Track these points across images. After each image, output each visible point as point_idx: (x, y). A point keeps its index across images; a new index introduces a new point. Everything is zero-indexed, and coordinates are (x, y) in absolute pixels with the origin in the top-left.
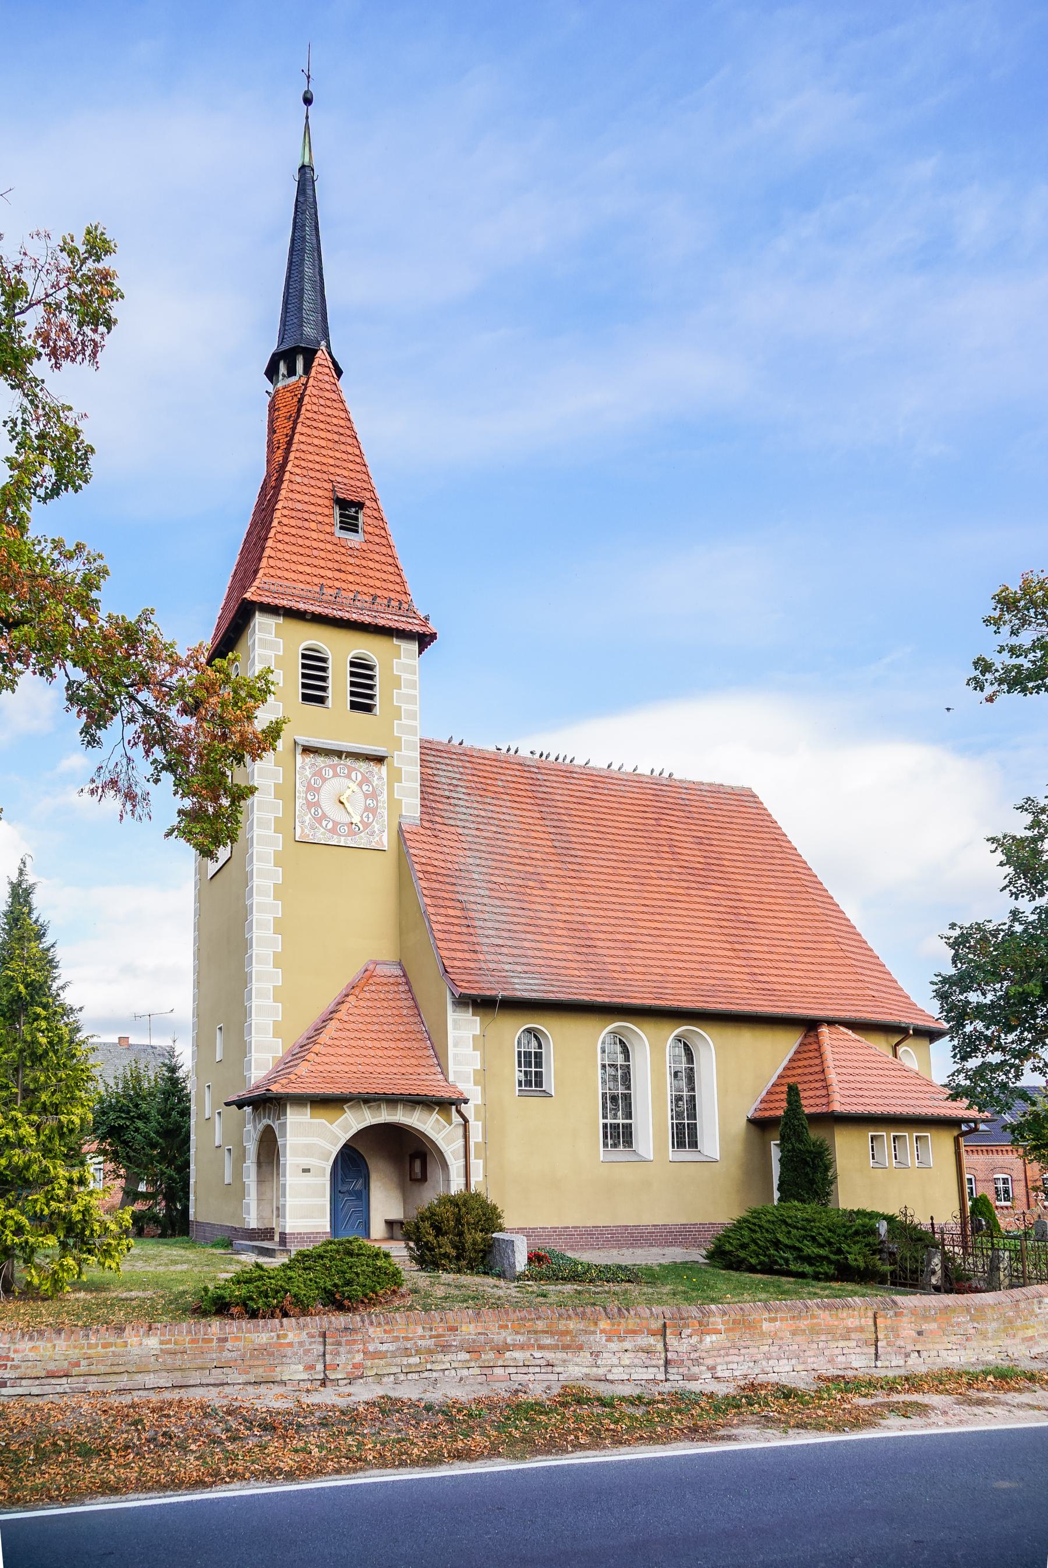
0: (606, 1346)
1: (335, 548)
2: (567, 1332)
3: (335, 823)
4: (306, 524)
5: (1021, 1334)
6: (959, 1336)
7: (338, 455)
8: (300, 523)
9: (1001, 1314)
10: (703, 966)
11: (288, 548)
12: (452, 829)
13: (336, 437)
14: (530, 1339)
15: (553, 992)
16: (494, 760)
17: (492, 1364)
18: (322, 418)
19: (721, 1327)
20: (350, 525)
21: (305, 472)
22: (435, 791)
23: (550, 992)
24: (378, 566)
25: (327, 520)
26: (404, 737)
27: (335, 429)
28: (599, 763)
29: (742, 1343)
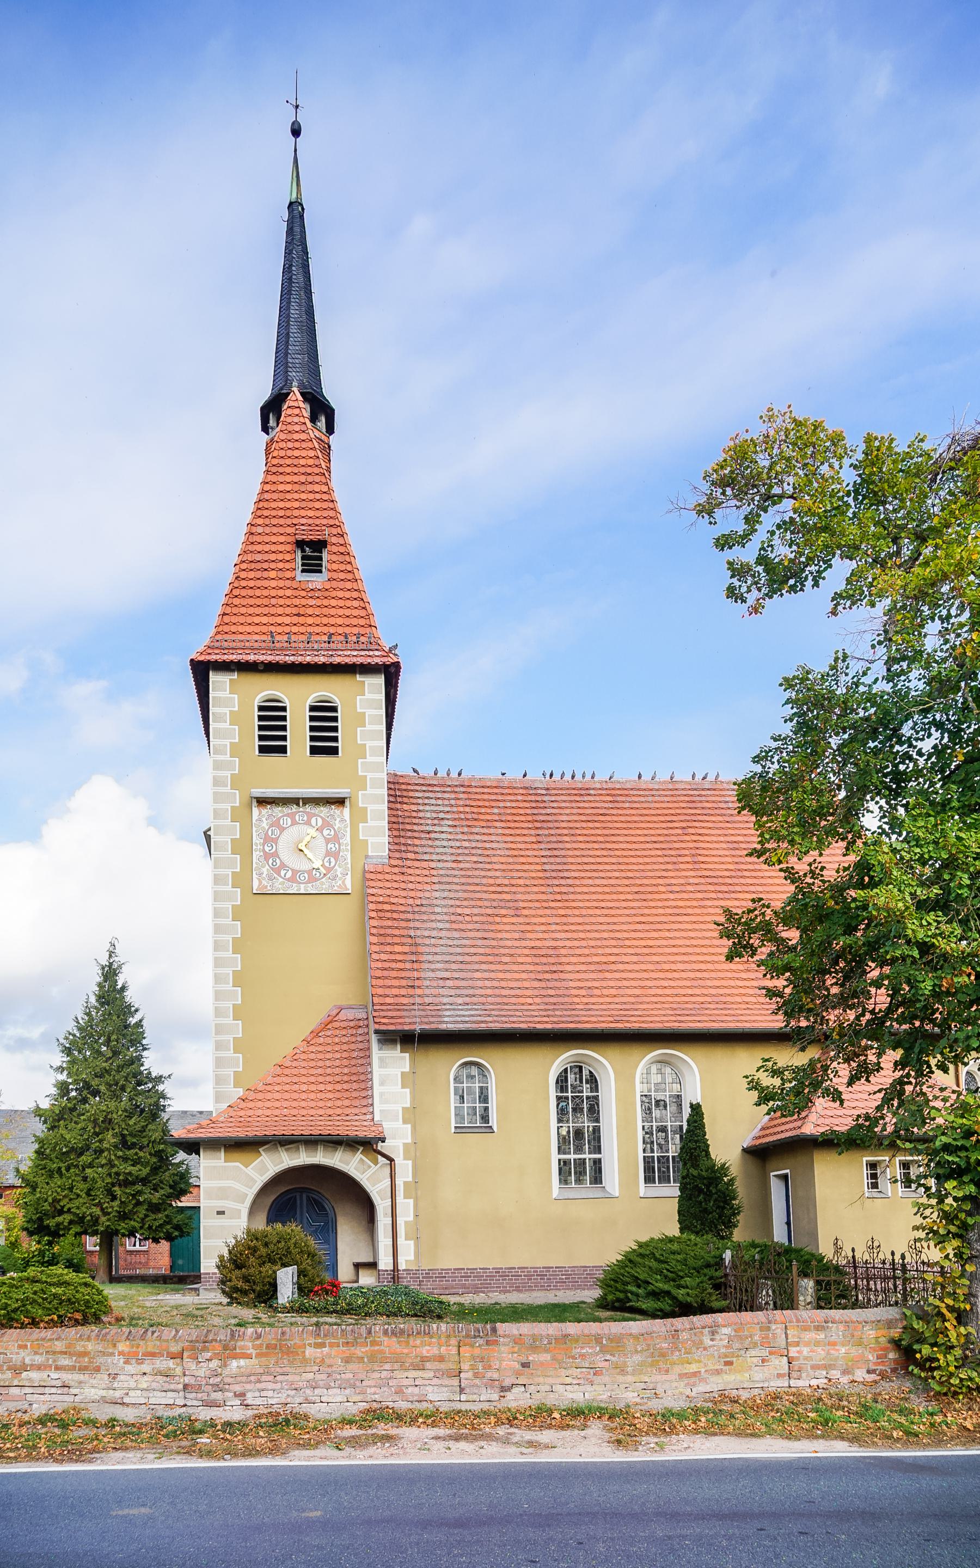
0: (123, 1368)
1: (296, 593)
2: (85, 1354)
3: (295, 872)
4: (265, 574)
5: (677, 1369)
6: (584, 1370)
7: (304, 496)
8: (259, 574)
9: (648, 1345)
10: (695, 983)
11: (244, 602)
12: (425, 864)
13: (303, 478)
14: (48, 1359)
15: (486, 1022)
16: (496, 787)
17: (7, 1384)
18: (289, 462)
19: (253, 1352)
20: (312, 566)
21: (267, 521)
22: (415, 828)
23: (482, 1022)
24: (341, 603)
25: (288, 566)
26: (370, 776)
27: (303, 470)
28: (626, 775)
29: (278, 1369)
